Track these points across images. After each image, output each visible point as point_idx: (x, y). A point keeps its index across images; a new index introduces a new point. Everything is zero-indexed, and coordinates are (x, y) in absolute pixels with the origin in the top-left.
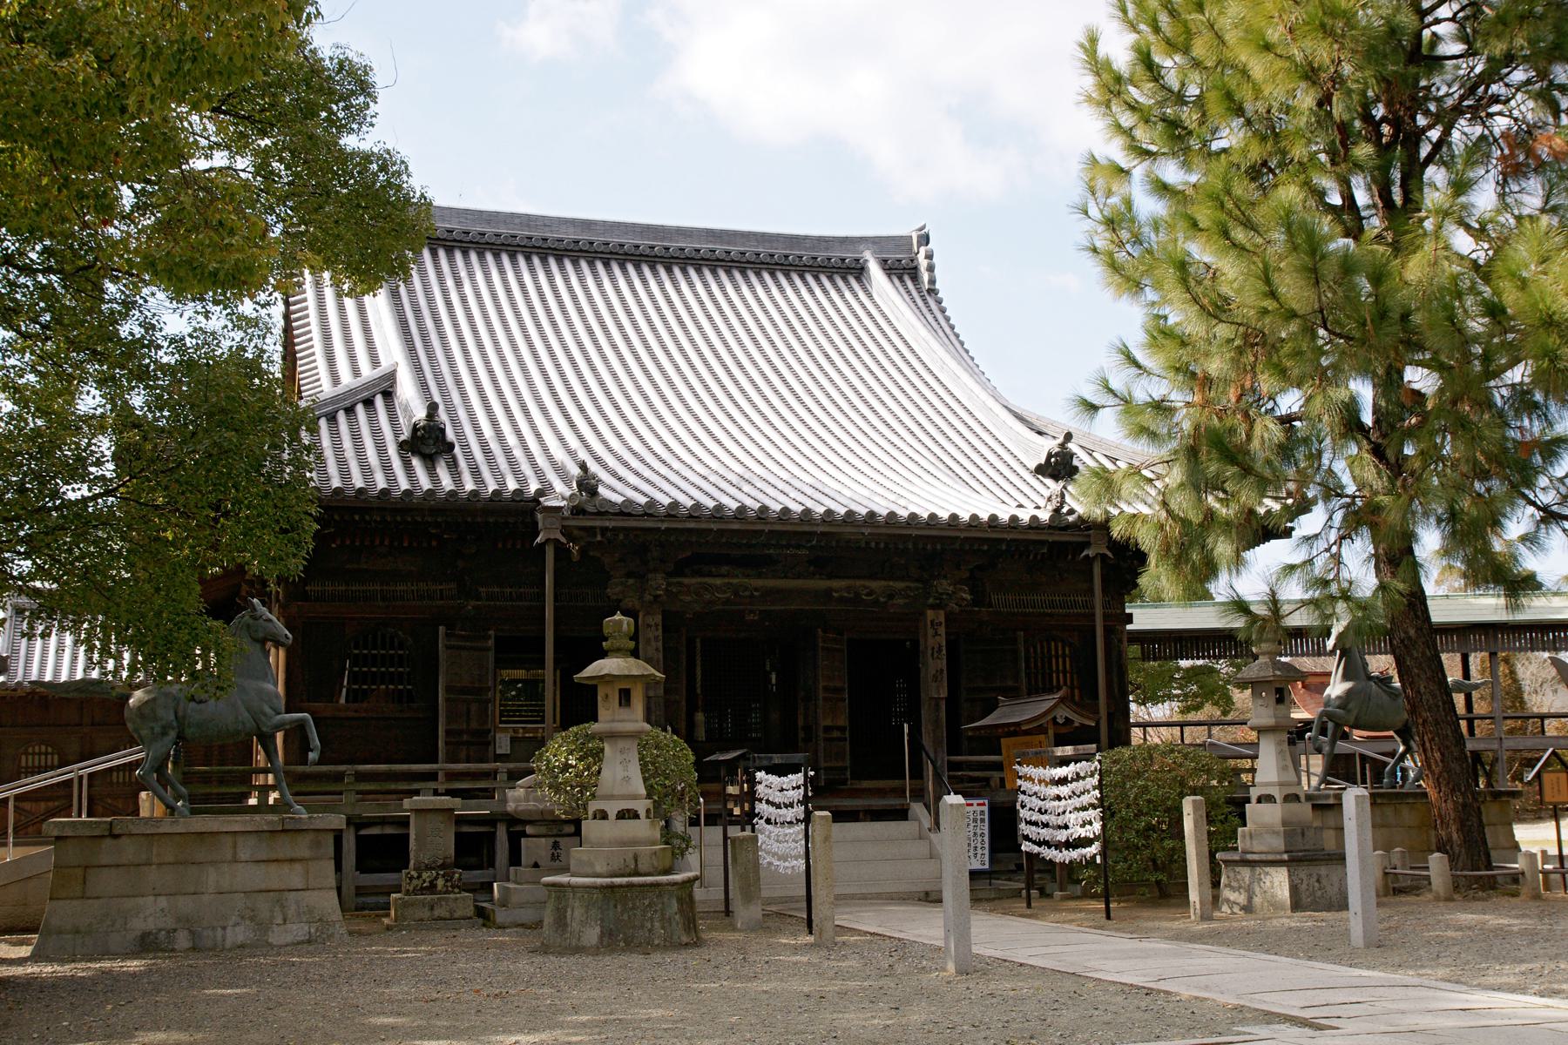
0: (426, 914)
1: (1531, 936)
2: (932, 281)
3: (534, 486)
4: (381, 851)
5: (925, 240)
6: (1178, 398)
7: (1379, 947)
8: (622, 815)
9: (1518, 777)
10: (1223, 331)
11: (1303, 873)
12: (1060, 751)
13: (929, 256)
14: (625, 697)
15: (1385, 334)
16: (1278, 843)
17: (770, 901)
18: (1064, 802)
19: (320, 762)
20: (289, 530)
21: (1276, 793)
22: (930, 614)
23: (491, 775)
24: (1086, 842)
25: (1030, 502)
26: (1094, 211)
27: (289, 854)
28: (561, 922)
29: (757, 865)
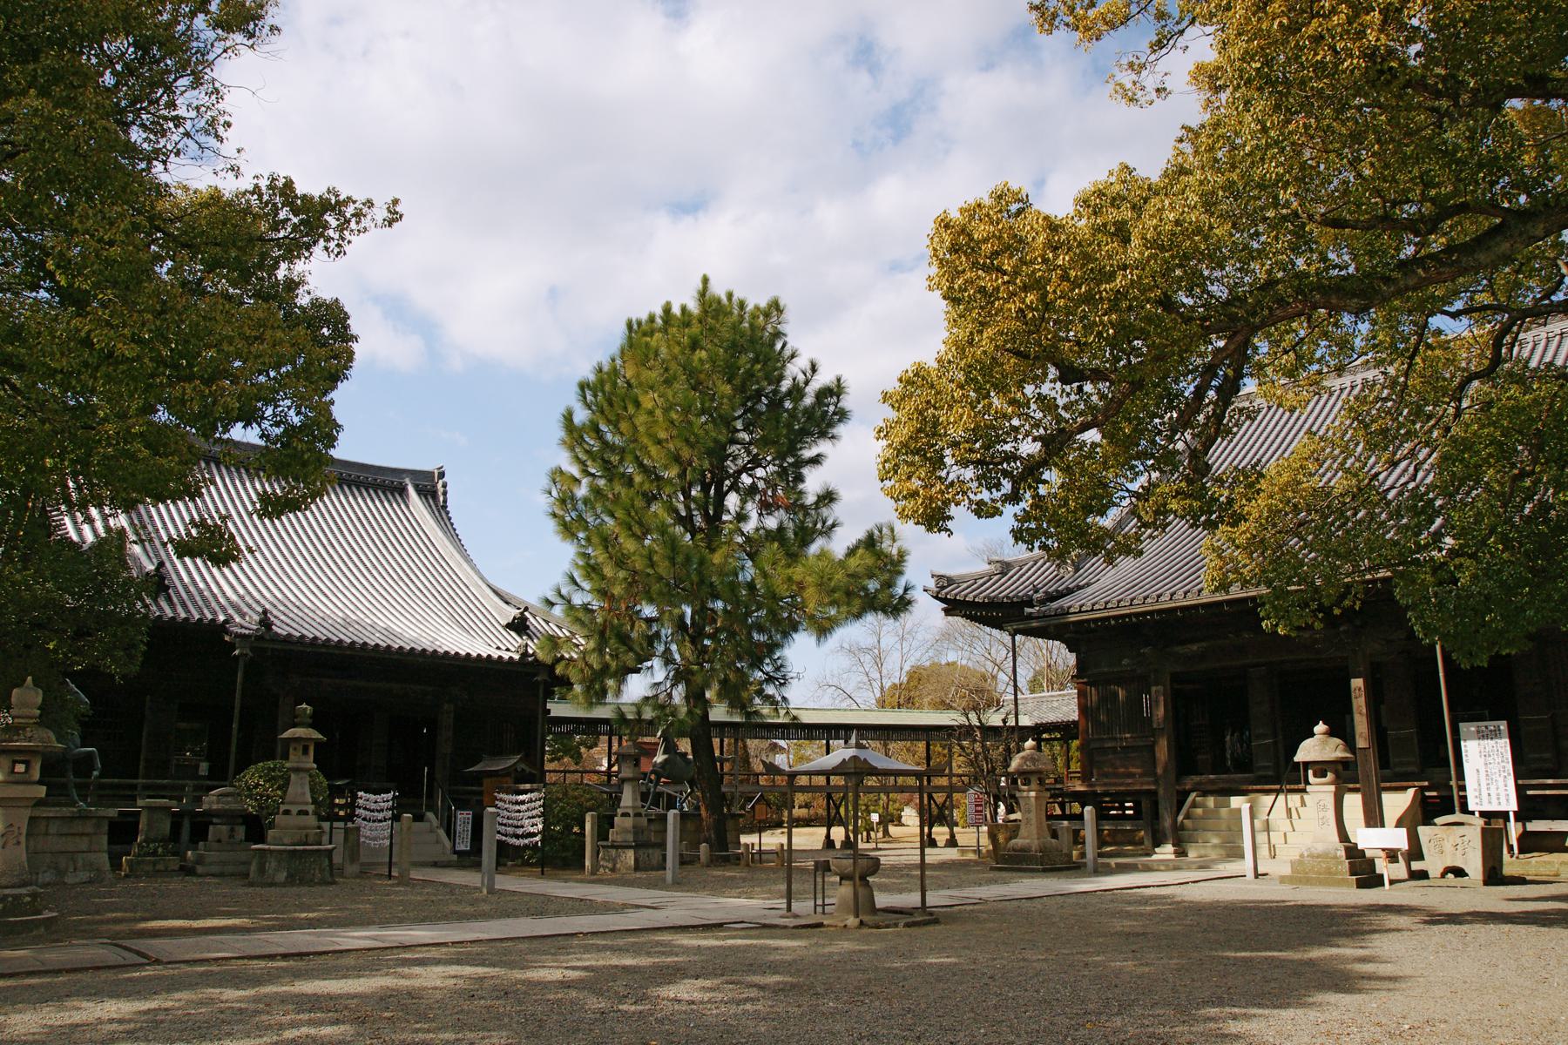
0: (150, 868)
1: (744, 880)
2: (445, 501)
3: (222, 618)
4: (122, 832)
5: (442, 475)
6: (595, 605)
7: (678, 884)
8: (300, 813)
9: (743, 807)
10: (622, 574)
11: (641, 852)
12: (522, 787)
13: (444, 486)
14: (305, 751)
15: (701, 588)
16: (630, 838)
17: (362, 864)
18: (522, 814)
19: (101, 776)
20: (129, 647)
21: (630, 811)
22: (446, 706)
23: (134, 787)
24: (533, 835)
25: (507, 647)
26: (554, 493)
27: (81, 829)
28: (262, 870)
29: (358, 844)
